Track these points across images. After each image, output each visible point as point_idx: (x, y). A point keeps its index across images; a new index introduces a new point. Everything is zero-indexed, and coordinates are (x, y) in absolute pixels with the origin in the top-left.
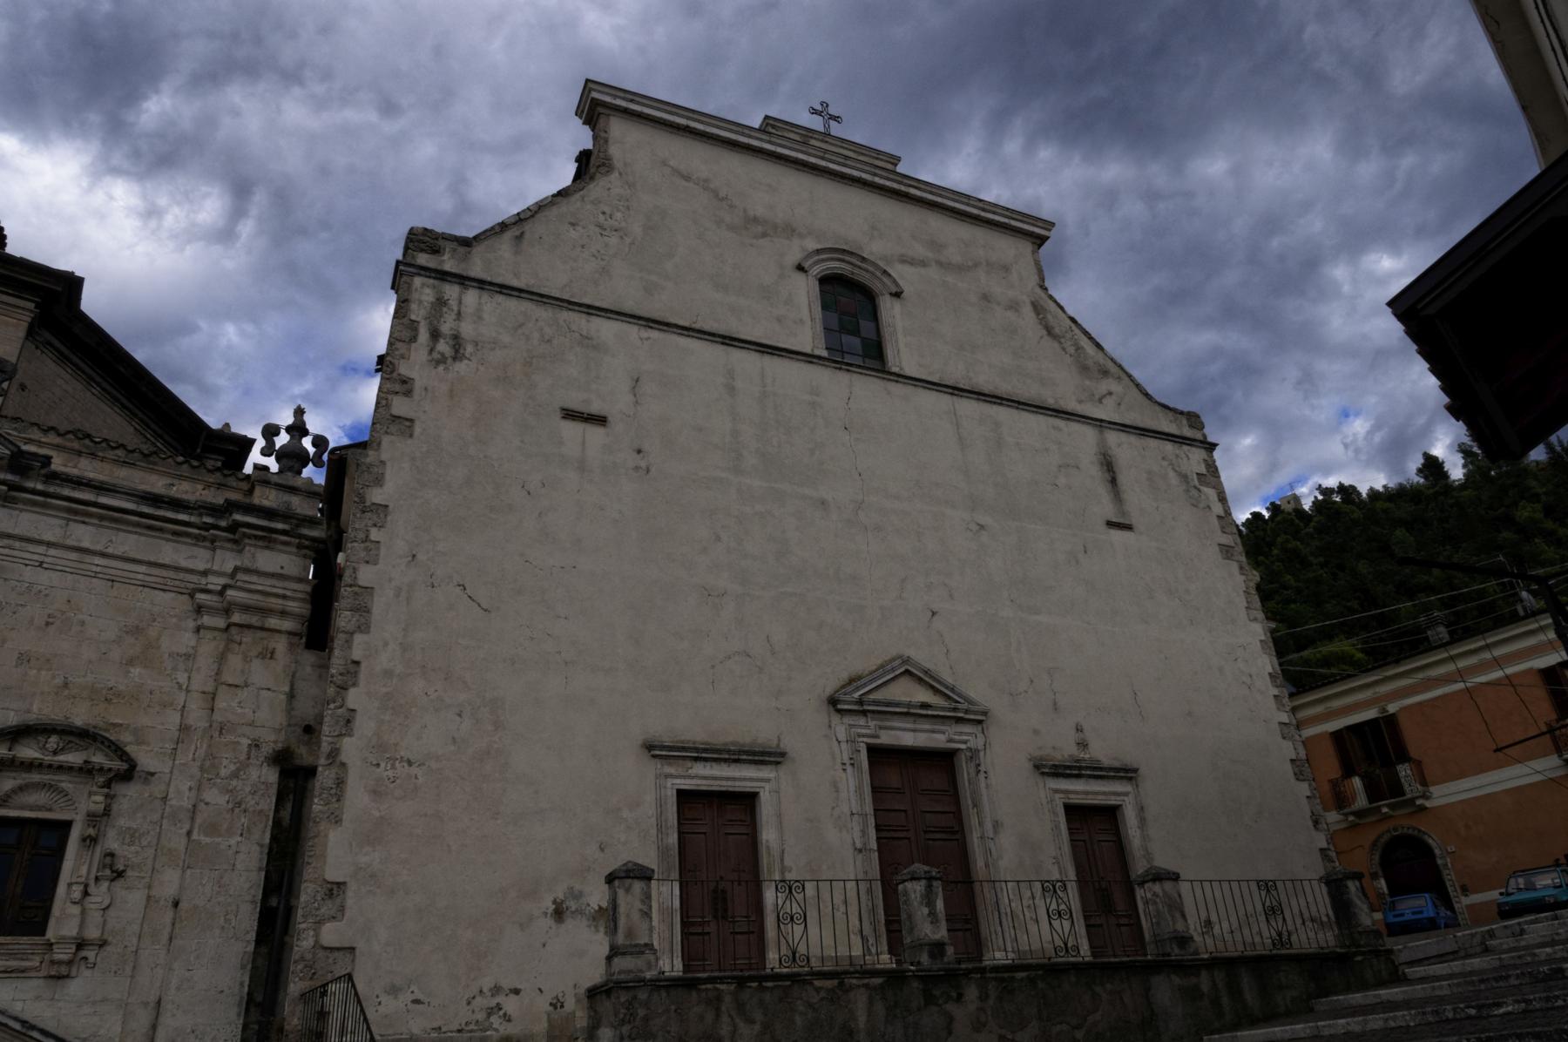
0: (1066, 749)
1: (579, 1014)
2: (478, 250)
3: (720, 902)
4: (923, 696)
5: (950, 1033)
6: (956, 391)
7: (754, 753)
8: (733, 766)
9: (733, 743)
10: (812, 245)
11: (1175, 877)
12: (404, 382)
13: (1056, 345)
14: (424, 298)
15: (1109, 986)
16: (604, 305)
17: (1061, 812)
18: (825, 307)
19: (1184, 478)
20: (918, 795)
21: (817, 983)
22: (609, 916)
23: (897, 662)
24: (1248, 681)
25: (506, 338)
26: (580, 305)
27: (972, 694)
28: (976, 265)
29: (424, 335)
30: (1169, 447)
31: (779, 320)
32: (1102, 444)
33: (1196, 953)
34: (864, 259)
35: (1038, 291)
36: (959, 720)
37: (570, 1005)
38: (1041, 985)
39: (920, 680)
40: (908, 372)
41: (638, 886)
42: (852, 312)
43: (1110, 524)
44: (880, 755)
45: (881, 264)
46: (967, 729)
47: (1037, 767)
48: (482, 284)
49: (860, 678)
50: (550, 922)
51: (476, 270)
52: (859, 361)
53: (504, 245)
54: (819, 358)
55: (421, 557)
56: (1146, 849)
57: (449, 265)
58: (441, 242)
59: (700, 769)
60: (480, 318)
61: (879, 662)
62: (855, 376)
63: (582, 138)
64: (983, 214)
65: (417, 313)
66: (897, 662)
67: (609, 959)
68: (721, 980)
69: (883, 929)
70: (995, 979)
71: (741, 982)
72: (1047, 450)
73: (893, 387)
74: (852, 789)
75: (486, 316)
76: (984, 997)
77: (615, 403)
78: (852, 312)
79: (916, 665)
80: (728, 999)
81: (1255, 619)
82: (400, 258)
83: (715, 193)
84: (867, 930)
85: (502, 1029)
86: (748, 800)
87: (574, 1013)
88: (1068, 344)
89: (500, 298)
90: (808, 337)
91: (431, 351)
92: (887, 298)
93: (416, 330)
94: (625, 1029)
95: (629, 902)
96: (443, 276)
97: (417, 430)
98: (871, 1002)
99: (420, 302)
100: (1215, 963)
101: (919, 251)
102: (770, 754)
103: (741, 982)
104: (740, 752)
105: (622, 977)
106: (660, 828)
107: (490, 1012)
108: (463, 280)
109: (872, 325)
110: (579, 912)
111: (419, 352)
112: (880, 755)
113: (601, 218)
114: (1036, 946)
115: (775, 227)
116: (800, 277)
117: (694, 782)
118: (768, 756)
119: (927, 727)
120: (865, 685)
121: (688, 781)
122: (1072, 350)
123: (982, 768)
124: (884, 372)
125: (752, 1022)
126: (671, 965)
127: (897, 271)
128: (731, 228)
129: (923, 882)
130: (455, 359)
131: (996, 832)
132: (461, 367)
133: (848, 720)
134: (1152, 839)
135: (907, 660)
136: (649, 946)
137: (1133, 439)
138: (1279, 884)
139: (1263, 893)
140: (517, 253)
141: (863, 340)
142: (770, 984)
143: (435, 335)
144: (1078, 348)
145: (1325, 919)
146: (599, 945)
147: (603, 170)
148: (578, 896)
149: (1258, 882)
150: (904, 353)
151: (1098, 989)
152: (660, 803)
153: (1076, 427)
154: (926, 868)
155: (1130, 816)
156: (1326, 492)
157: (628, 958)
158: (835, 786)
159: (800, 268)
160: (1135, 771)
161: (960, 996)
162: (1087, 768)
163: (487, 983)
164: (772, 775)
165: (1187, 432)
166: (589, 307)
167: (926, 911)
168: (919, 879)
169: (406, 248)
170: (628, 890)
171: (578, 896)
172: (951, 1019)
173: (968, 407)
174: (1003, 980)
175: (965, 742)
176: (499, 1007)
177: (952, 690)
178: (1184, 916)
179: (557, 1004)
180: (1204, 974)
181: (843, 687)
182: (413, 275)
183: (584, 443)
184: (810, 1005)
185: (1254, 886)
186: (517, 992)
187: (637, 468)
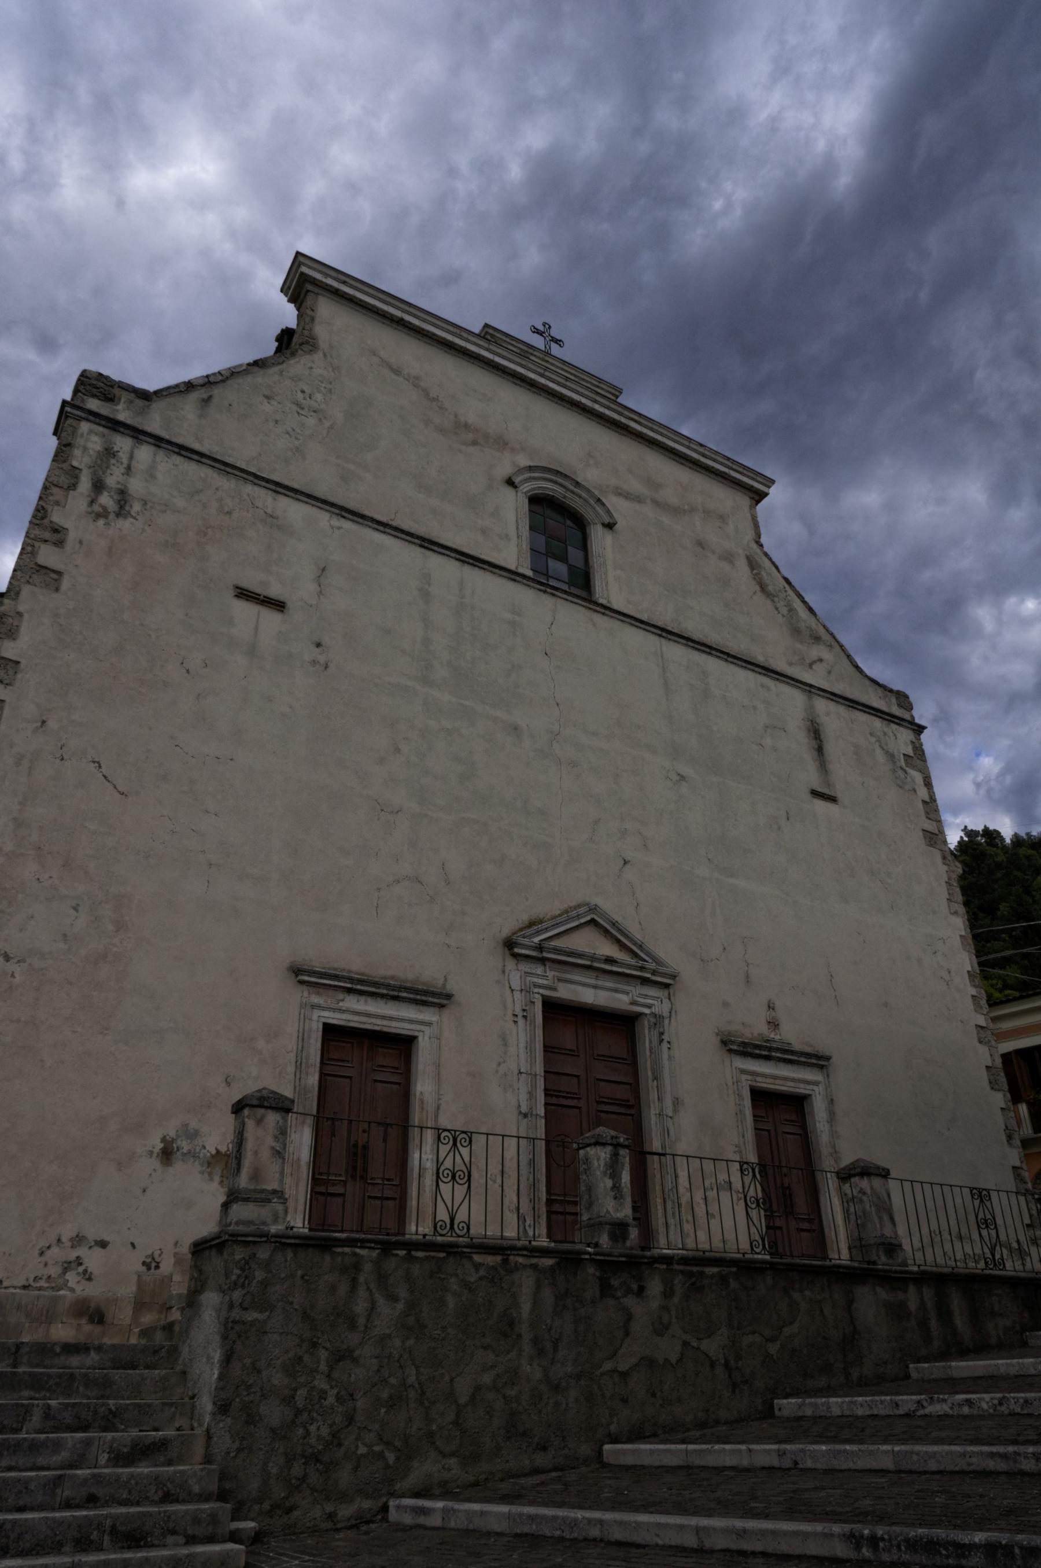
0: (756, 1028)
1: (177, 1278)
2: (158, 406)
3: (358, 1160)
4: (607, 949)
5: (627, 1334)
6: (664, 632)
7: (417, 992)
8: (391, 1003)
9: (393, 978)
10: (524, 461)
11: (884, 1174)
12: (56, 531)
13: (769, 602)
14: (90, 445)
15: (807, 1293)
16: (296, 486)
17: (747, 1094)
18: (532, 528)
19: (891, 757)
20: (594, 1056)
21: (477, 1258)
22: (230, 1161)
23: (582, 910)
24: (947, 978)
25: (180, 503)
26: (268, 481)
27: (661, 954)
28: (692, 510)
29: (85, 484)
30: (877, 723)
31: (484, 531)
32: (810, 710)
33: (905, 1263)
34: (577, 484)
35: (755, 546)
36: (645, 981)
37: (167, 1266)
38: (733, 1284)
39: (606, 932)
40: (615, 606)
41: (272, 1118)
42: (562, 534)
43: (815, 793)
44: (556, 1011)
45: (596, 492)
46: (652, 992)
47: (724, 1043)
48: (158, 441)
49: (541, 921)
50: (155, 1163)
51: (154, 423)
52: (565, 587)
53: (189, 406)
54: (524, 576)
55: (52, 724)
56: (834, 1147)
57: (123, 414)
58: (116, 391)
59: (352, 1003)
60: (153, 477)
61: (565, 906)
62: (559, 601)
63: (288, 315)
64: (703, 459)
65: (79, 459)
66: (582, 910)
67: (226, 1206)
68: (363, 1243)
69: (543, 1210)
70: (682, 1272)
71: (387, 1248)
72: (755, 708)
73: (598, 619)
74: (522, 1045)
75: (159, 476)
76: (668, 1293)
77: (299, 591)
78: (562, 534)
79: (604, 915)
80: (368, 1267)
81: (956, 913)
82: (68, 398)
83: (426, 392)
84: (525, 1207)
85: (78, 1289)
86: (403, 1045)
87: (170, 1277)
88: (781, 604)
89: (178, 460)
90: (513, 553)
91: (92, 502)
92: (599, 527)
93: (77, 477)
94: (237, 1295)
95: (261, 1134)
96: (115, 425)
97: (65, 584)
98: (538, 1287)
99: (85, 449)
100: (923, 1278)
101: (636, 486)
102: (433, 994)
103: (387, 1248)
104: (401, 988)
105: (241, 1228)
106: (299, 1066)
107: (67, 1266)
108: (137, 434)
109: (580, 554)
110: (192, 1155)
111: (78, 501)
112: (556, 1011)
113: (300, 396)
114: (717, 1244)
115: (487, 437)
116: (509, 492)
117: (344, 1016)
118: (432, 997)
119: (609, 985)
120: (547, 930)
121: (338, 1015)
122: (784, 610)
123: (665, 1037)
124: (591, 601)
125: (394, 1298)
126: (298, 1222)
127: (612, 501)
128: (441, 430)
129: (609, 1149)
130: (118, 515)
131: (675, 1111)
132: (125, 525)
133: (525, 967)
134: (841, 1135)
135: (594, 909)
136: (279, 1194)
137: (841, 710)
138: (993, 1194)
139: (977, 1202)
140: (201, 416)
141: (571, 567)
142: (420, 1254)
143: (98, 486)
144: (791, 610)
145: (1015, 1245)
146: (213, 1194)
147: (306, 347)
148: (193, 1135)
149: (971, 1189)
150: (612, 585)
151: (796, 1296)
152: (302, 1038)
153: (785, 689)
154: (613, 1133)
155: (819, 1107)
156: (970, 833)
157: (251, 1206)
158: (504, 1039)
159: (510, 482)
160: (828, 1058)
161: (642, 1289)
162: (778, 1050)
163: (67, 1231)
164: (434, 1019)
165: (896, 710)
166: (277, 484)
167: (609, 1183)
168: (604, 1144)
169: (76, 391)
170: (259, 1122)
171: (193, 1135)
172: (629, 1317)
173: (676, 652)
174: (691, 1274)
175: (649, 1006)
176: (79, 1261)
177: (640, 947)
178: (892, 1219)
179: (151, 1264)
180: (912, 1288)
181: (521, 930)
182: (80, 419)
183: (256, 629)
184: (466, 1285)
185: (966, 1191)
186: (103, 1244)
187: (314, 662)
